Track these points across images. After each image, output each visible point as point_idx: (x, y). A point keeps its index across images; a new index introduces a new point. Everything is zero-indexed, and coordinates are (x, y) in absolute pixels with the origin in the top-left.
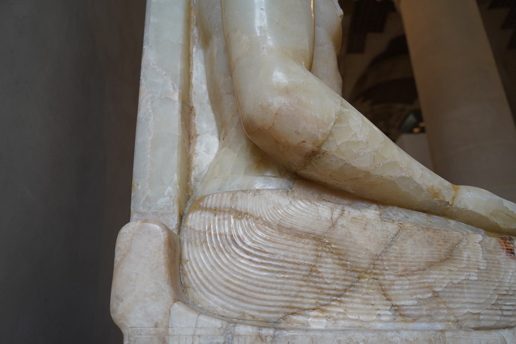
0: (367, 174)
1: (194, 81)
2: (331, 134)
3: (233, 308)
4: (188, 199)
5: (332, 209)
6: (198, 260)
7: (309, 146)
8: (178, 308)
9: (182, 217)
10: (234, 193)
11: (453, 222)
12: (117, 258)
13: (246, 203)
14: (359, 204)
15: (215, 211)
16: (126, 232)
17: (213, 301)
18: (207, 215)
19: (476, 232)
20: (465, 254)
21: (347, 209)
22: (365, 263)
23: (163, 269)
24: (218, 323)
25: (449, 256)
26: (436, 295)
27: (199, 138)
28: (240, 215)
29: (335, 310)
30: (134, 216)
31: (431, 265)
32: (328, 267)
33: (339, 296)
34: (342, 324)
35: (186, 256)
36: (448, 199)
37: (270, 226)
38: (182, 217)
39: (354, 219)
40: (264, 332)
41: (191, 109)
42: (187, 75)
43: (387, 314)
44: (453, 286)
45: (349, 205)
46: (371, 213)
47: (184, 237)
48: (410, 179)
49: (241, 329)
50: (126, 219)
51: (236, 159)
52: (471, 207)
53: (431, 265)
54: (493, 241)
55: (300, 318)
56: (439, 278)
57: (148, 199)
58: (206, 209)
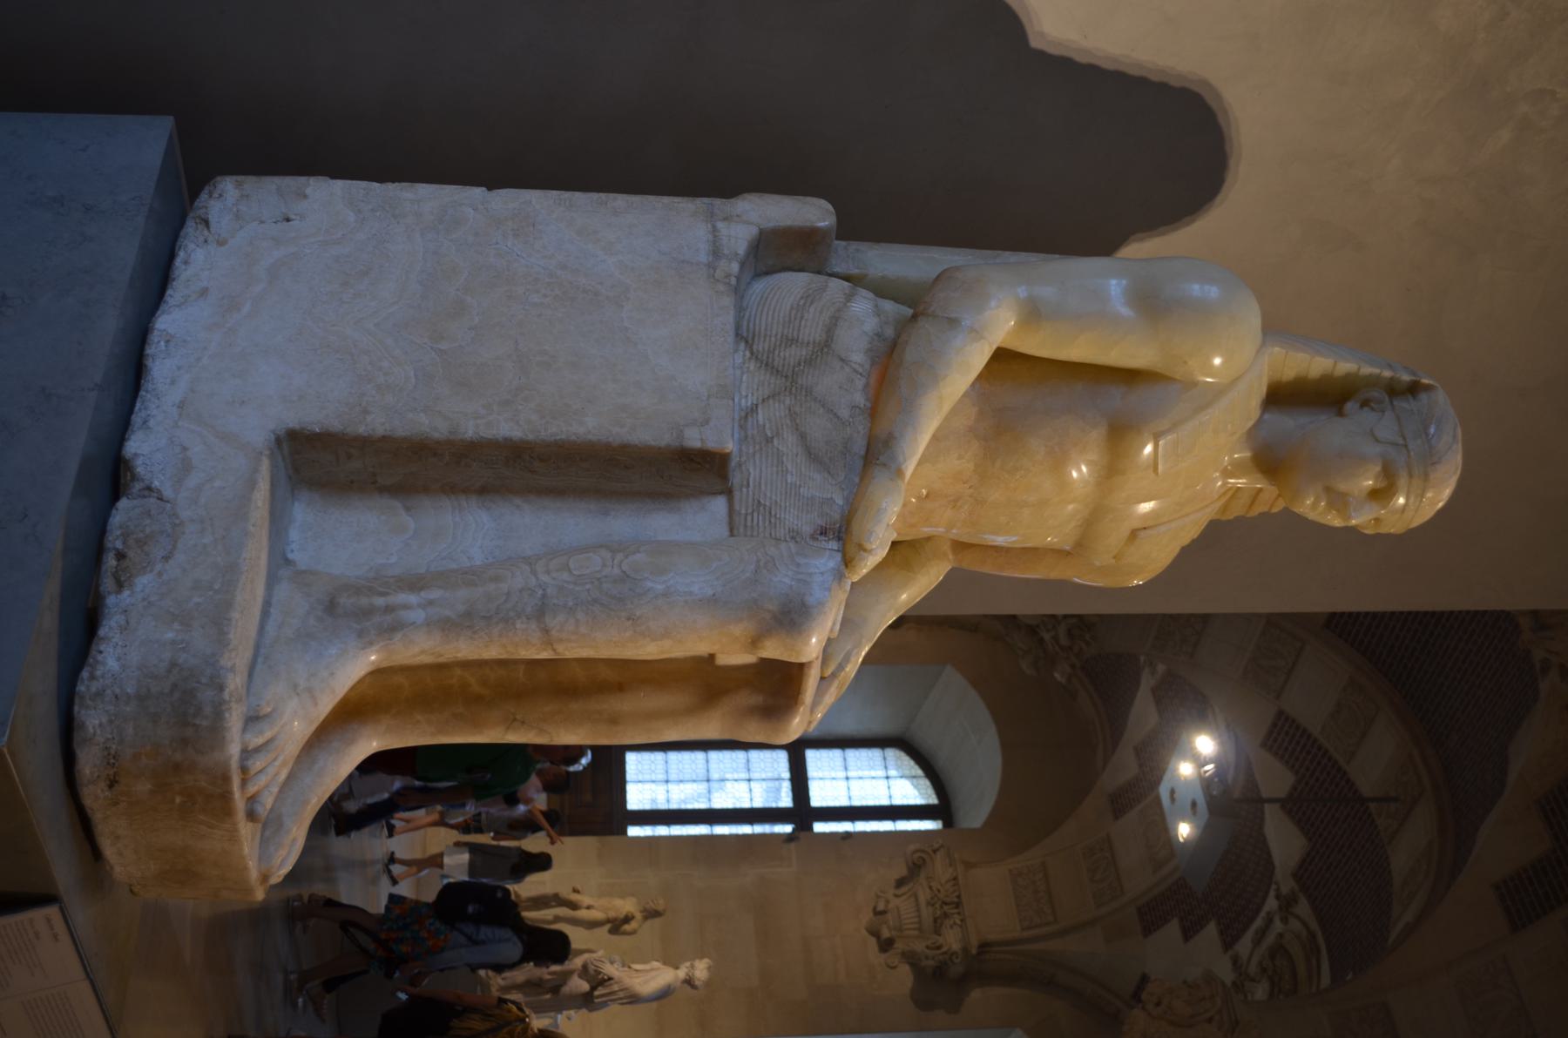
25: (812, 456)
26: (769, 440)
31: (803, 437)
32: (792, 354)
53: (803, 437)
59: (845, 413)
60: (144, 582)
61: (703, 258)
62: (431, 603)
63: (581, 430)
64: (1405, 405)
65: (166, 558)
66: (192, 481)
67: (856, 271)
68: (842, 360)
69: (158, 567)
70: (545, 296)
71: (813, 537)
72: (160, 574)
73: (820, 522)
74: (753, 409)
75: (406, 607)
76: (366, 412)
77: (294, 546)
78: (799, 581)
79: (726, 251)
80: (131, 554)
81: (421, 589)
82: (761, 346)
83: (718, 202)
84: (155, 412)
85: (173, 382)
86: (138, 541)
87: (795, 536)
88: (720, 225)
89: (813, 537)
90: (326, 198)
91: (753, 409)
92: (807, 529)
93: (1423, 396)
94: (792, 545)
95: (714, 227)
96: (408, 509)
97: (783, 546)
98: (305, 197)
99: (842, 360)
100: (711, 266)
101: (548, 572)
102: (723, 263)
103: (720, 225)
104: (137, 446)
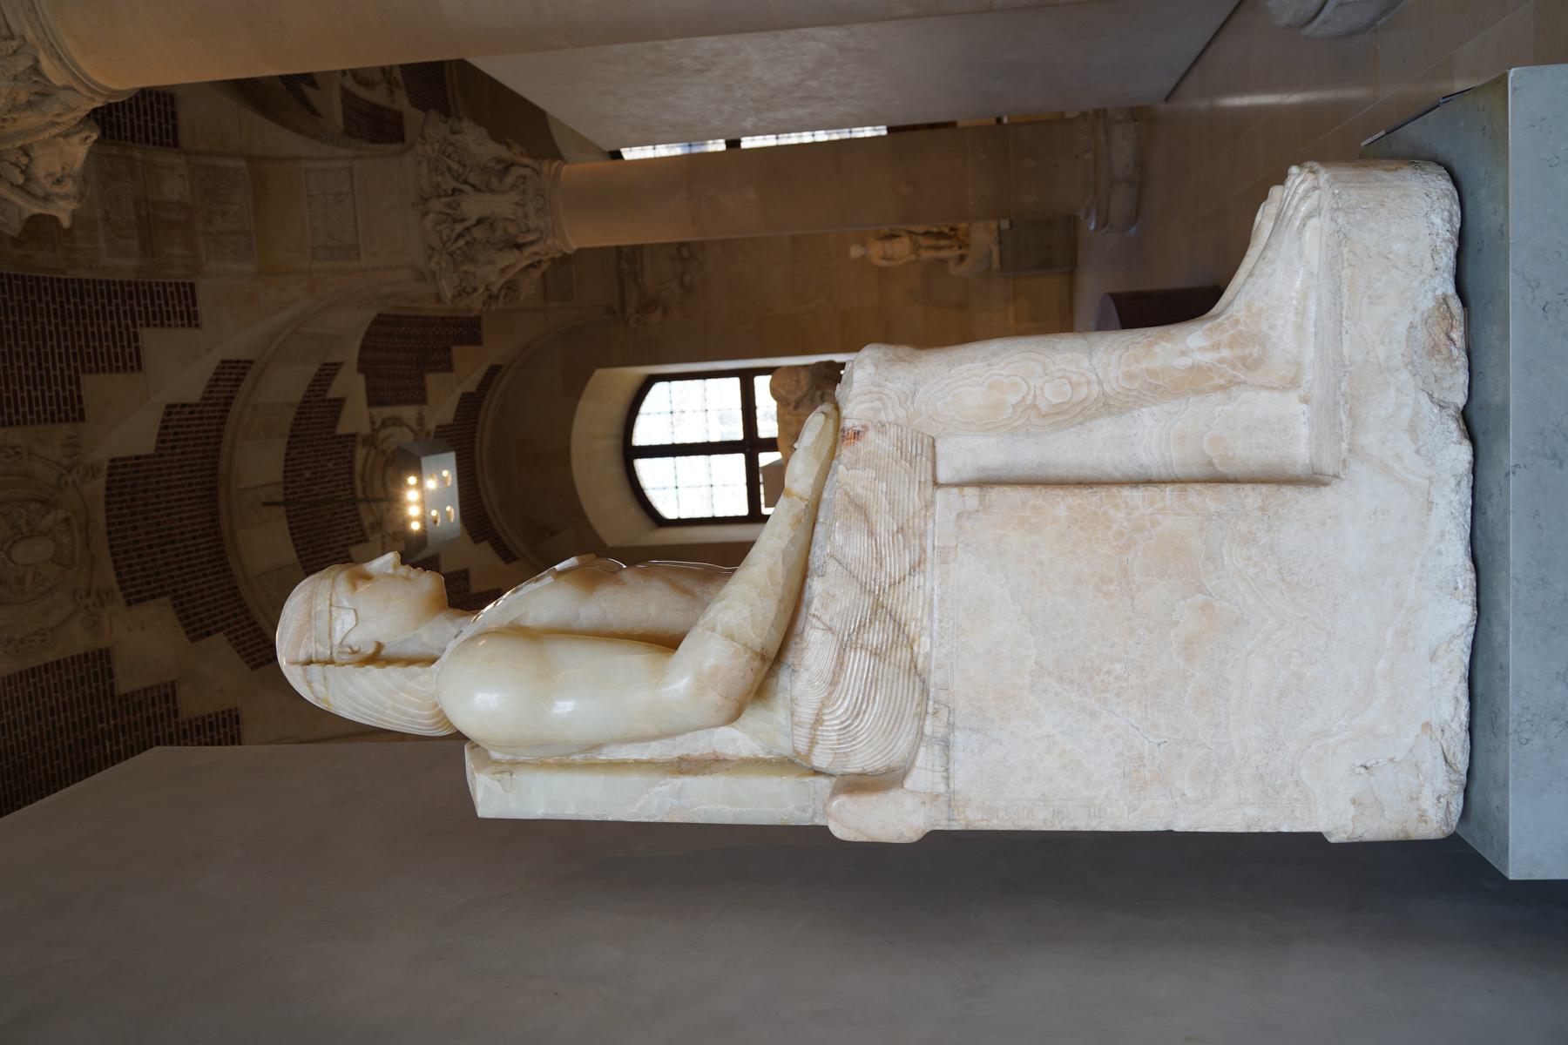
0: (781, 601)
1: (645, 757)
2: (745, 645)
3: (909, 726)
4: (792, 765)
5: (814, 627)
6: (862, 760)
7: (757, 664)
8: (908, 784)
9: (817, 772)
10: (794, 724)
11: (825, 495)
12: (864, 839)
13: (806, 712)
14: (807, 596)
15: (813, 742)
16: (839, 831)
17: (903, 744)
18: (817, 750)
19: (836, 472)
20: (860, 491)
21: (812, 611)
22: (868, 601)
23: (875, 799)
24: (923, 750)
25: (862, 509)
26: (901, 530)
27: (719, 750)
28: (818, 720)
29: (912, 629)
30: (819, 821)
31: (871, 533)
32: (874, 637)
33: (900, 626)
34: (925, 623)
35: (859, 770)
36: (802, 505)
37: (831, 694)
38: (817, 772)
39: (824, 606)
40: (930, 710)
41: (681, 759)
42: (638, 765)
43: (918, 579)
44: (892, 511)
45: (808, 607)
46: (816, 586)
47: (838, 770)
48: (784, 552)
49: (928, 730)
50: (825, 830)
51: (754, 719)
52: (811, 481)
53: (871, 533)
54: (845, 453)
55: (920, 660)
56: (884, 524)
57: (798, 809)
58: (810, 751)
59: (832, 567)
60: (1427, 303)
61: (959, 738)
62: (1183, 353)
63: (1070, 500)
64: (321, 649)
65: (1412, 326)
66: (1406, 413)
67: (807, 779)
68: (830, 629)
69: (1417, 318)
70: (1108, 672)
71: (866, 428)
72: (1415, 310)
73: (859, 444)
74: (913, 570)
75: (1202, 349)
76: (1263, 509)
77: (1303, 419)
78: (879, 386)
79: (937, 747)
80: (1425, 719)
81: (1192, 368)
82: (904, 654)
83: (943, 825)
84: (1452, 497)
85: (1442, 534)
86: (1439, 352)
87: (882, 428)
88: (941, 788)
89: (866, 428)
90: (1338, 820)
91: (913, 570)
92: (871, 435)
93: (302, 657)
94: (884, 418)
95: (948, 785)
96: (1210, 464)
97: (892, 418)
98: (1354, 802)
99: (830, 629)
100: (951, 726)
101: (1089, 382)
102: (941, 732)
103: (941, 788)
104: (1464, 453)
